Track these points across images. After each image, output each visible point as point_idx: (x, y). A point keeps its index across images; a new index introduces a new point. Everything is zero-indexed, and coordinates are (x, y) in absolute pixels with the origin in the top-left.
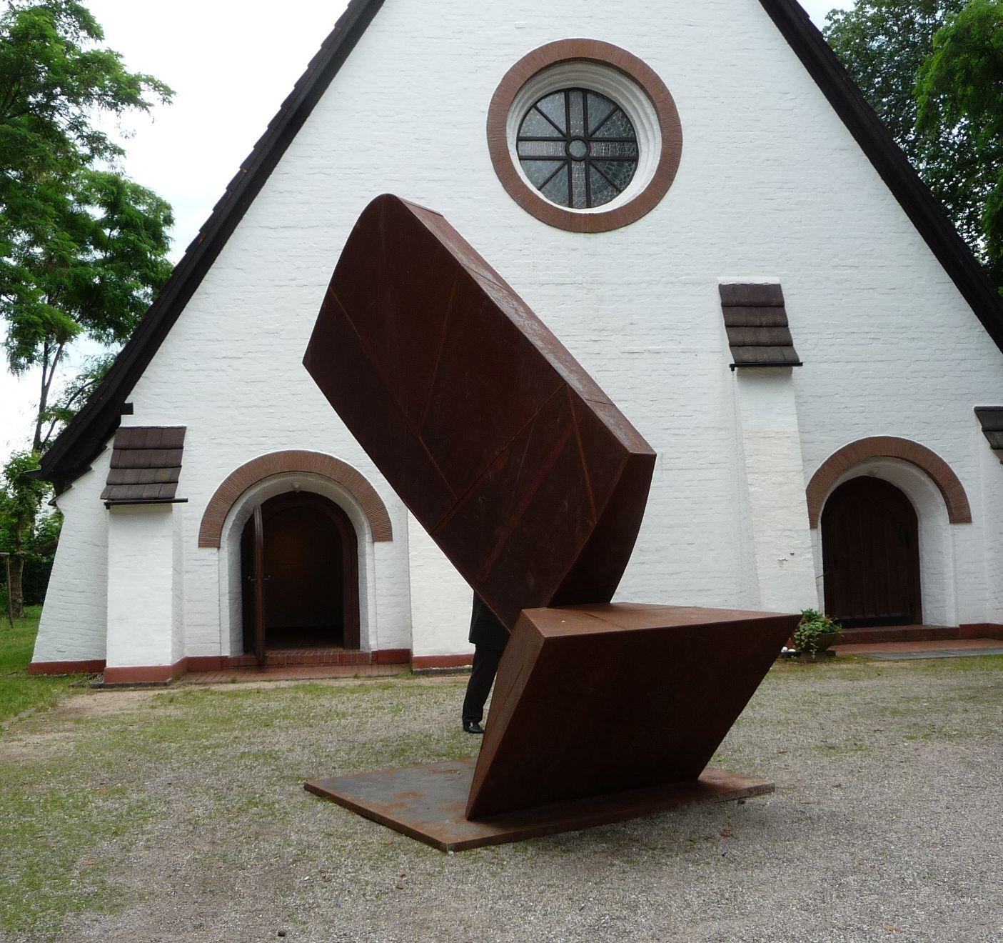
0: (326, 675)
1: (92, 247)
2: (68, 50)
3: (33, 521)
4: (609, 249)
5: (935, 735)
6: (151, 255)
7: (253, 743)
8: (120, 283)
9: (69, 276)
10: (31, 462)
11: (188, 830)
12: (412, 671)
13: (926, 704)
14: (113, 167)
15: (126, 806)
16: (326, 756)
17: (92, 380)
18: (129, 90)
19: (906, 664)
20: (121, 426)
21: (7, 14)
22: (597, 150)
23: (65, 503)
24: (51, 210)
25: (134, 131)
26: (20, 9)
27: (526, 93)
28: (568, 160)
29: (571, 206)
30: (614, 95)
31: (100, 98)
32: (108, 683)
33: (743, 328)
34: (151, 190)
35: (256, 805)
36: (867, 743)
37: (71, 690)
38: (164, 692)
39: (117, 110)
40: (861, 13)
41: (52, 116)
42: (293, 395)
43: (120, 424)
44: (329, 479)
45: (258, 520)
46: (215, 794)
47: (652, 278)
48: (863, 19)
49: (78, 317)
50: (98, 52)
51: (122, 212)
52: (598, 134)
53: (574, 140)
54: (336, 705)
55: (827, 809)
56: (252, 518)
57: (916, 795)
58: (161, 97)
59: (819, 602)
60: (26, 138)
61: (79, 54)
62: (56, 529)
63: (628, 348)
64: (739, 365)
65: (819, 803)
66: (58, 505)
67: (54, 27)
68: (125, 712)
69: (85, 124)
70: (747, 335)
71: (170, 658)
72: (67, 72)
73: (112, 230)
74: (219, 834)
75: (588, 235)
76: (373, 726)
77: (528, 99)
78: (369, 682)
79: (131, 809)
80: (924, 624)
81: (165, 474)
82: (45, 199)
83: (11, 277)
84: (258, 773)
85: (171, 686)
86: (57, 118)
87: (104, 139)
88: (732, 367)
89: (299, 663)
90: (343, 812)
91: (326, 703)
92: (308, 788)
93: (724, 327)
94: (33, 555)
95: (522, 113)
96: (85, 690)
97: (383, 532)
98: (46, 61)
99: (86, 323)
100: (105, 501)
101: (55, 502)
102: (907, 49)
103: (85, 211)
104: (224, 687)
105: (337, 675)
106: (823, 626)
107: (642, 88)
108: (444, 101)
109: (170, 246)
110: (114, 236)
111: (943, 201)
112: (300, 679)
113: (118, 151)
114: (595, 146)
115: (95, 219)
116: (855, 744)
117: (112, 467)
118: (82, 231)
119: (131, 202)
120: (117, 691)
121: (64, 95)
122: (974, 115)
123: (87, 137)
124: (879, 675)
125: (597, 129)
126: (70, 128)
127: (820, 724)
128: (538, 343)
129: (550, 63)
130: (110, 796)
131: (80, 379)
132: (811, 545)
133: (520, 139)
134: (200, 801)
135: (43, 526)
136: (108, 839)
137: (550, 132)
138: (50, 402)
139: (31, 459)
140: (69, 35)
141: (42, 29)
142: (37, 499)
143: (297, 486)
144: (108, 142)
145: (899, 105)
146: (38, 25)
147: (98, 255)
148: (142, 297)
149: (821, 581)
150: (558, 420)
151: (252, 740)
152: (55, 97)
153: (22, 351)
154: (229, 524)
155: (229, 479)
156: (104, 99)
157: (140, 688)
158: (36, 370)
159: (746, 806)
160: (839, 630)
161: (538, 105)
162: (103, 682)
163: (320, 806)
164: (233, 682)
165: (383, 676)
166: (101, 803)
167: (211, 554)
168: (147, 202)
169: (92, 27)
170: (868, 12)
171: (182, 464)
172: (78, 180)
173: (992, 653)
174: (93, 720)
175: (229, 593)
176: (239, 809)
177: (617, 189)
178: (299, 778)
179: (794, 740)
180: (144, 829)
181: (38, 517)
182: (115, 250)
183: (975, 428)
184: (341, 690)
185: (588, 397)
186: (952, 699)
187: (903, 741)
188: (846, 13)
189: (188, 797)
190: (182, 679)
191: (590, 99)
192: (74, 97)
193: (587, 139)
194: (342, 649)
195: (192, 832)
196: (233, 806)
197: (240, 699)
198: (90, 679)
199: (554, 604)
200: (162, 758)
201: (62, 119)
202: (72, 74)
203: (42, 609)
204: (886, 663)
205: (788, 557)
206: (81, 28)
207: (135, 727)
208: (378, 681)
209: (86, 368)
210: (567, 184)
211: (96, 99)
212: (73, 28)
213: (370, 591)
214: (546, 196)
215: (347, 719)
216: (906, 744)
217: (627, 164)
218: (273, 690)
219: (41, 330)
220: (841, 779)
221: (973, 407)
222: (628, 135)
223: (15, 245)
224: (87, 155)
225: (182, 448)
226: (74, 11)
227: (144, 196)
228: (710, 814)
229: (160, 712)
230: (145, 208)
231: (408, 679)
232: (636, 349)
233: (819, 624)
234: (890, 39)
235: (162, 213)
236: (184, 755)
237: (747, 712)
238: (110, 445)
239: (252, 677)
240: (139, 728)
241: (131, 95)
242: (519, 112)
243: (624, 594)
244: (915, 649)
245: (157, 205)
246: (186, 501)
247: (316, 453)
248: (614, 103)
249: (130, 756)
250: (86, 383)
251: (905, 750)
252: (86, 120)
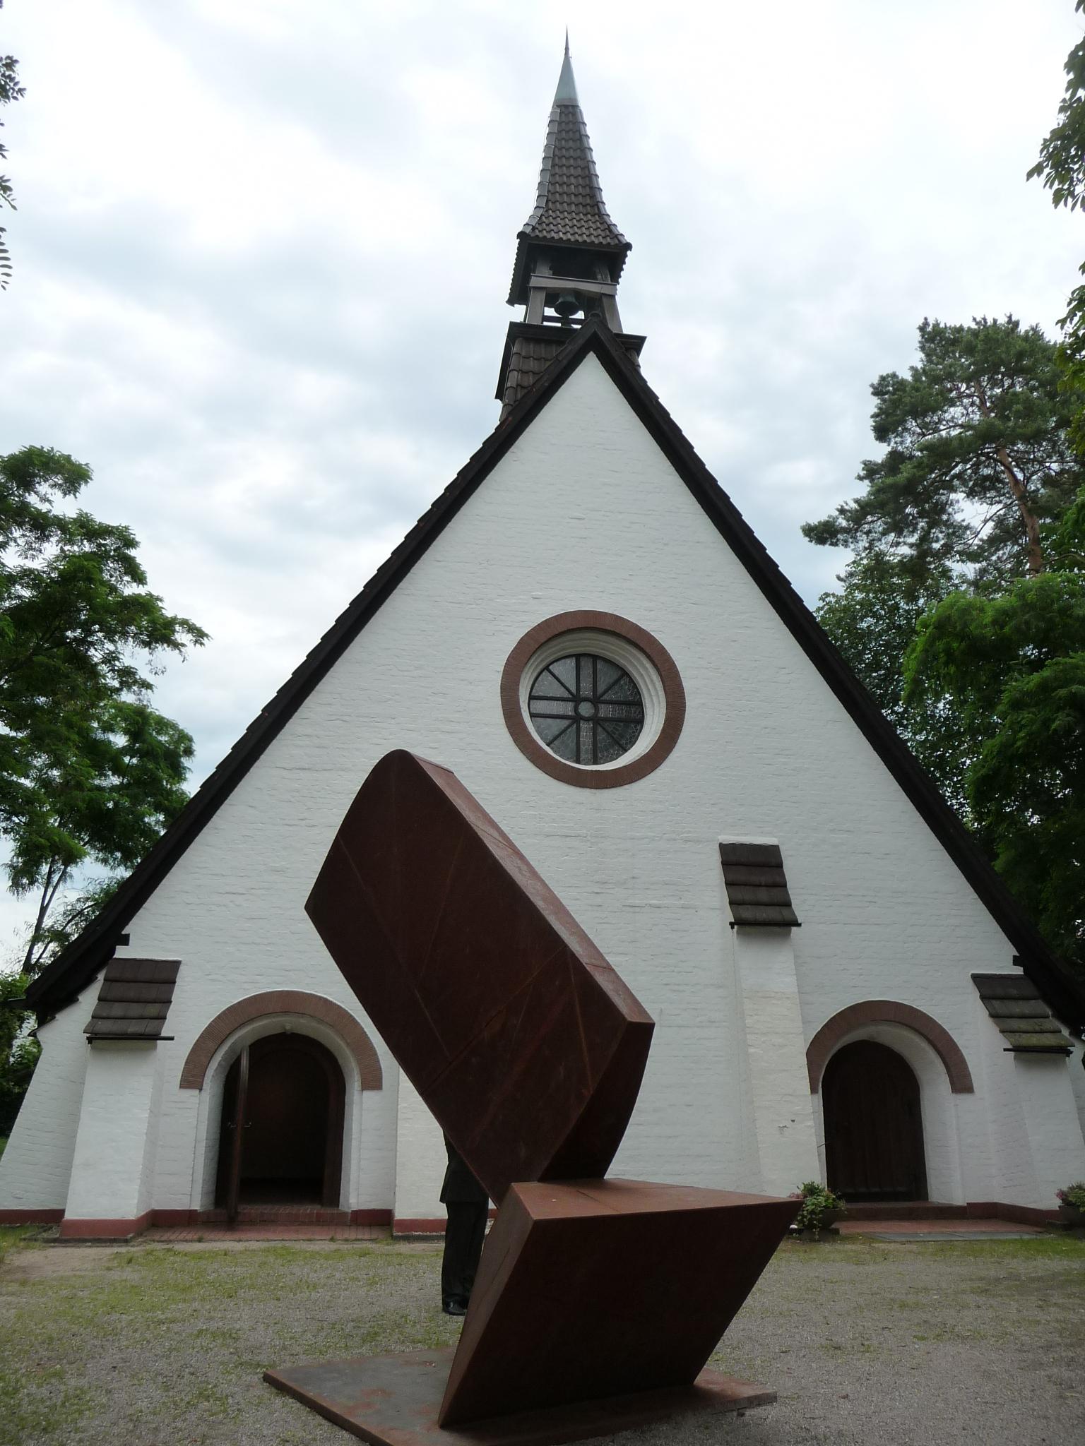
0: (301, 1237)
1: (110, 773)
2: (111, 593)
3: (11, 1046)
4: (614, 804)
5: (947, 1336)
6: (167, 785)
7: (212, 1318)
8: (133, 809)
9: (84, 801)
10: (18, 984)
11: (127, 1429)
12: (392, 1236)
13: (936, 1297)
14: (140, 700)
15: (62, 1394)
16: (291, 1338)
17: (93, 903)
18: (164, 631)
19: (914, 1247)
20: (114, 957)
21: (58, 557)
22: (604, 711)
23: (45, 1035)
24: (75, 737)
25: (165, 668)
26: (71, 554)
27: (539, 656)
28: (576, 719)
29: (578, 762)
30: (622, 662)
31: (135, 637)
32: (64, 1237)
33: (742, 887)
34: (174, 722)
35: (207, 1398)
36: (875, 1343)
37: (22, 1244)
38: (123, 1250)
39: (150, 648)
40: (850, 597)
41: (87, 650)
42: (293, 933)
43: (114, 953)
44: (321, 1021)
45: (245, 1063)
46: (163, 1383)
47: (654, 834)
48: (853, 603)
49: (87, 840)
50: (140, 595)
51: (143, 742)
52: (606, 697)
53: (583, 701)
54: (308, 1274)
55: (834, 1427)
56: (238, 1060)
57: (929, 1411)
58: (194, 639)
59: (821, 1174)
60: (60, 669)
61: (121, 596)
62: (34, 1056)
63: (630, 902)
64: (738, 923)
65: (825, 1418)
66: (38, 1037)
67: (101, 571)
68: (78, 1273)
69: (118, 659)
70: (747, 894)
71: (135, 1211)
72: (106, 612)
73: (131, 758)
74: (162, 1435)
76: (345, 1301)
77: (542, 661)
78: (345, 1246)
79: (67, 1398)
80: (929, 1200)
81: (152, 1010)
82: (70, 725)
83: (25, 799)
84: (214, 1357)
85: (131, 1244)
86: (92, 652)
87: (134, 674)
88: (732, 925)
89: (273, 1221)
90: (303, 1411)
91: (296, 1270)
92: (268, 1379)
93: (724, 885)
94: (5, 1084)
95: (535, 674)
96: (37, 1244)
97: (373, 1081)
98: (89, 600)
99: (95, 846)
100: (88, 1035)
101: (35, 1033)
102: (894, 631)
103: (108, 738)
104: (188, 1246)
105: (312, 1237)
106: (825, 1201)
107: (649, 657)
108: (462, 660)
109: (187, 776)
110: (133, 764)
111: (932, 769)
112: (272, 1240)
113: (147, 686)
114: (603, 708)
115: (117, 747)
116: (862, 1344)
117: (99, 999)
118: (102, 757)
119: (154, 733)
120: (73, 1247)
121: (101, 632)
122: (959, 691)
123: (117, 671)
124: (885, 1259)
125: (605, 692)
126: (103, 662)
127: (825, 1317)
128: (539, 903)
129: (563, 630)
130: (45, 1380)
131: (80, 902)
132: (812, 1111)
133: (531, 698)
134: (145, 1392)
135: (20, 1053)
136: (36, 1437)
137: (561, 692)
138: (47, 923)
139: (18, 981)
140: (114, 579)
141: (89, 572)
142: (18, 1023)
143: (288, 1027)
144: (138, 677)
145: (888, 679)
146: (86, 569)
147: (116, 780)
148: (153, 823)
149: (823, 1149)
150: (557, 983)
151: (212, 1314)
152: (92, 633)
153: (22, 875)
154: (214, 1065)
155: (219, 1017)
156: (139, 638)
157: (98, 1245)
158: (36, 893)
159: (746, 1418)
160: (842, 1205)
161: (551, 667)
162: (58, 1236)
163: (279, 1401)
164: (200, 1240)
165: (361, 1240)
166: (34, 1390)
167: (192, 1096)
168: (169, 734)
169: (136, 573)
170: (857, 597)
171: (172, 1000)
172: (105, 709)
173: (1001, 1237)
174: (41, 1283)
175: (207, 1139)
176: (188, 1403)
177: (623, 748)
178: (258, 1365)
179: (797, 1336)
180: (79, 1425)
181: (16, 1043)
182: (132, 776)
183: (973, 994)
184: (314, 1255)
185: (588, 962)
186: (964, 1292)
187: (913, 1342)
188: (837, 596)
189: (133, 1385)
190: (144, 1234)
191: (600, 665)
192: (110, 635)
193: (596, 701)
194: (319, 1207)
195: (132, 1431)
196: (182, 1400)
197: (205, 1262)
198: (45, 1231)
199: (547, 1177)
200: (111, 1334)
201: (96, 654)
202: (112, 613)
203: (6, 1143)
204: (892, 1244)
205: (789, 1124)
206: (126, 573)
207: (86, 1293)
208: (355, 1246)
209: (88, 891)
210: (575, 741)
211: (133, 637)
212: (118, 573)
213: (354, 1143)
214: (555, 752)
215: (318, 1292)
216: (917, 1346)
217: (633, 726)
218: (241, 1252)
219: (47, 852)
220: (849, 1389)
221: (970, 974)
222: (634, 699)
223: (35, 767)
224: (117, 688)
225: (174, 982)
226: (121, 559)
227: (167, 728)
228: (707, 1428)
229: (116, 1275)
230: (166, 739)
231: (388, 1245)
232: (637, 902)
233: (821, 1199)
234: (878, 621)
235: (182, 745)
236: (135, 1331)
237: (749, 1301)
238: (101, 977)
239: (220, 1235)
240: (89, 1294)
241: (166, 636)
242: (530, 678)
243: (617, 1170)
244: (923, 1230)
245: (179, 736)
246: (172, 1039)
247: (311, 994)
248: (622, 669)
249: (75, 1329)
250: (86, 906)
251: (916, 1353)
252: (121, 656)
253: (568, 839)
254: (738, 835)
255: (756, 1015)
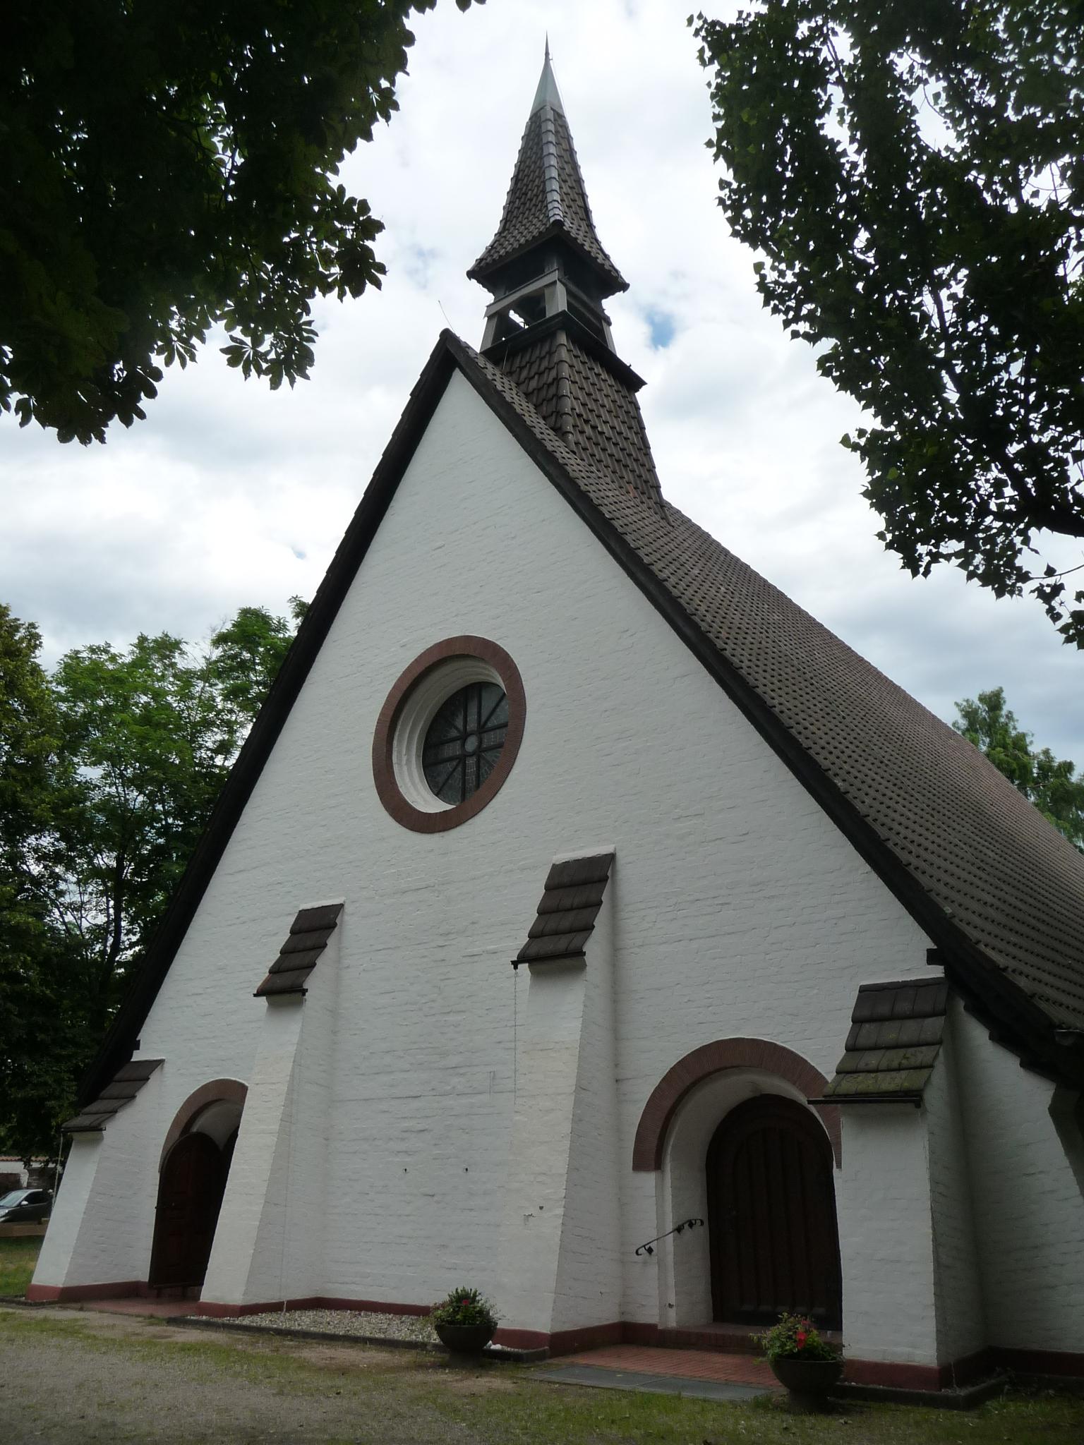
75: (441, 834)
171: (267, 974)
183: (626, 276)
205: (535, 1211)
232: (476, 950)
253: (420, 891)
254: (574, 850)
255: (530, 1073)
